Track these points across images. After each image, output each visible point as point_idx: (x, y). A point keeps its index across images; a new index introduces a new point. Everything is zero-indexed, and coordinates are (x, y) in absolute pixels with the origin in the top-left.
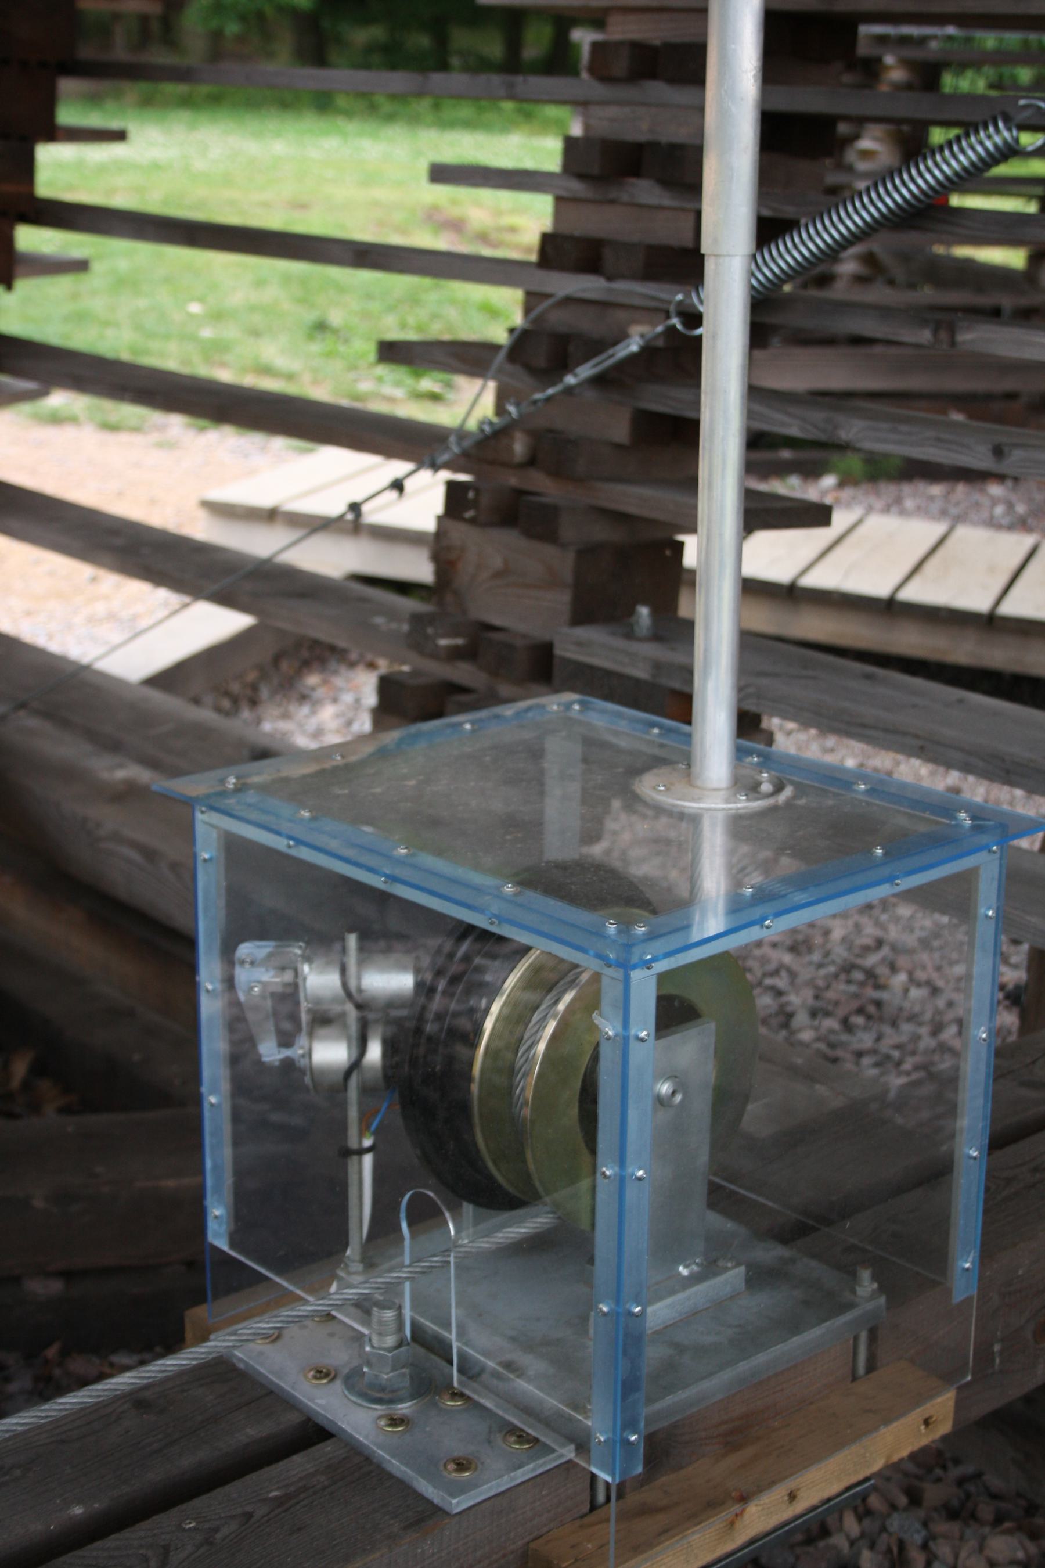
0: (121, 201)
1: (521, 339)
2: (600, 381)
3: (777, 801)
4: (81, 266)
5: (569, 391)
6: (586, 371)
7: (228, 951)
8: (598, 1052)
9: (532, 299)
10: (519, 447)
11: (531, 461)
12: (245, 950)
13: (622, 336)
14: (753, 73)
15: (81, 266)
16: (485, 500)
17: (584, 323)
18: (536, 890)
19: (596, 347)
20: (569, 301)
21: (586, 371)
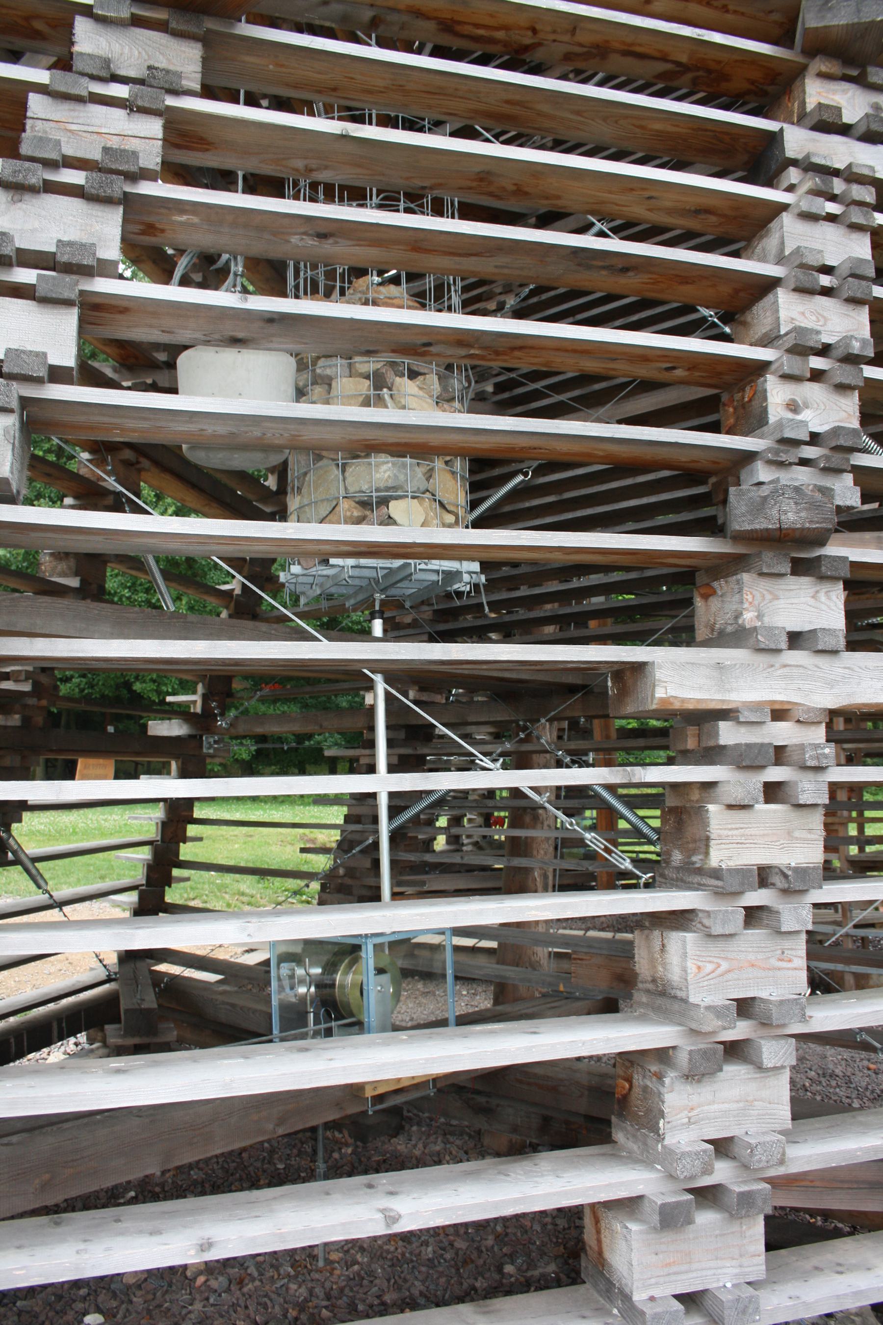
0: (99, 809)
1: (340, 844)
2: (361, 851)
3: (509, 860)
4: (188, 879)
5: (354, 854)
6: (358, 849)
7: (278, 968)
8: (847, 1109)
9: (342, 832)
10: (341, 871)
11: (345, 875)
12: (282, 965)
13: (368, 839)
14: (558, 448)
15: (188, 879)
16: (332, 886)
17: (357, 837)
18: (759, 869)
19: (360, 843)
20: (352, 832)
21: (358, 849)
